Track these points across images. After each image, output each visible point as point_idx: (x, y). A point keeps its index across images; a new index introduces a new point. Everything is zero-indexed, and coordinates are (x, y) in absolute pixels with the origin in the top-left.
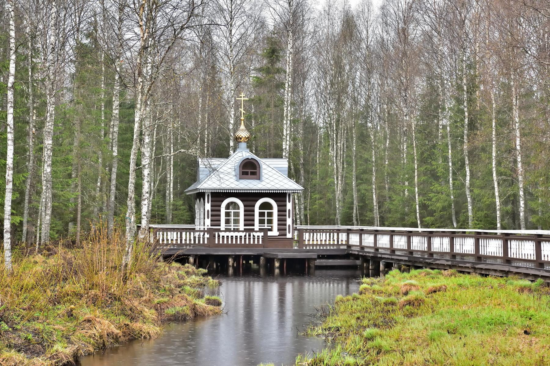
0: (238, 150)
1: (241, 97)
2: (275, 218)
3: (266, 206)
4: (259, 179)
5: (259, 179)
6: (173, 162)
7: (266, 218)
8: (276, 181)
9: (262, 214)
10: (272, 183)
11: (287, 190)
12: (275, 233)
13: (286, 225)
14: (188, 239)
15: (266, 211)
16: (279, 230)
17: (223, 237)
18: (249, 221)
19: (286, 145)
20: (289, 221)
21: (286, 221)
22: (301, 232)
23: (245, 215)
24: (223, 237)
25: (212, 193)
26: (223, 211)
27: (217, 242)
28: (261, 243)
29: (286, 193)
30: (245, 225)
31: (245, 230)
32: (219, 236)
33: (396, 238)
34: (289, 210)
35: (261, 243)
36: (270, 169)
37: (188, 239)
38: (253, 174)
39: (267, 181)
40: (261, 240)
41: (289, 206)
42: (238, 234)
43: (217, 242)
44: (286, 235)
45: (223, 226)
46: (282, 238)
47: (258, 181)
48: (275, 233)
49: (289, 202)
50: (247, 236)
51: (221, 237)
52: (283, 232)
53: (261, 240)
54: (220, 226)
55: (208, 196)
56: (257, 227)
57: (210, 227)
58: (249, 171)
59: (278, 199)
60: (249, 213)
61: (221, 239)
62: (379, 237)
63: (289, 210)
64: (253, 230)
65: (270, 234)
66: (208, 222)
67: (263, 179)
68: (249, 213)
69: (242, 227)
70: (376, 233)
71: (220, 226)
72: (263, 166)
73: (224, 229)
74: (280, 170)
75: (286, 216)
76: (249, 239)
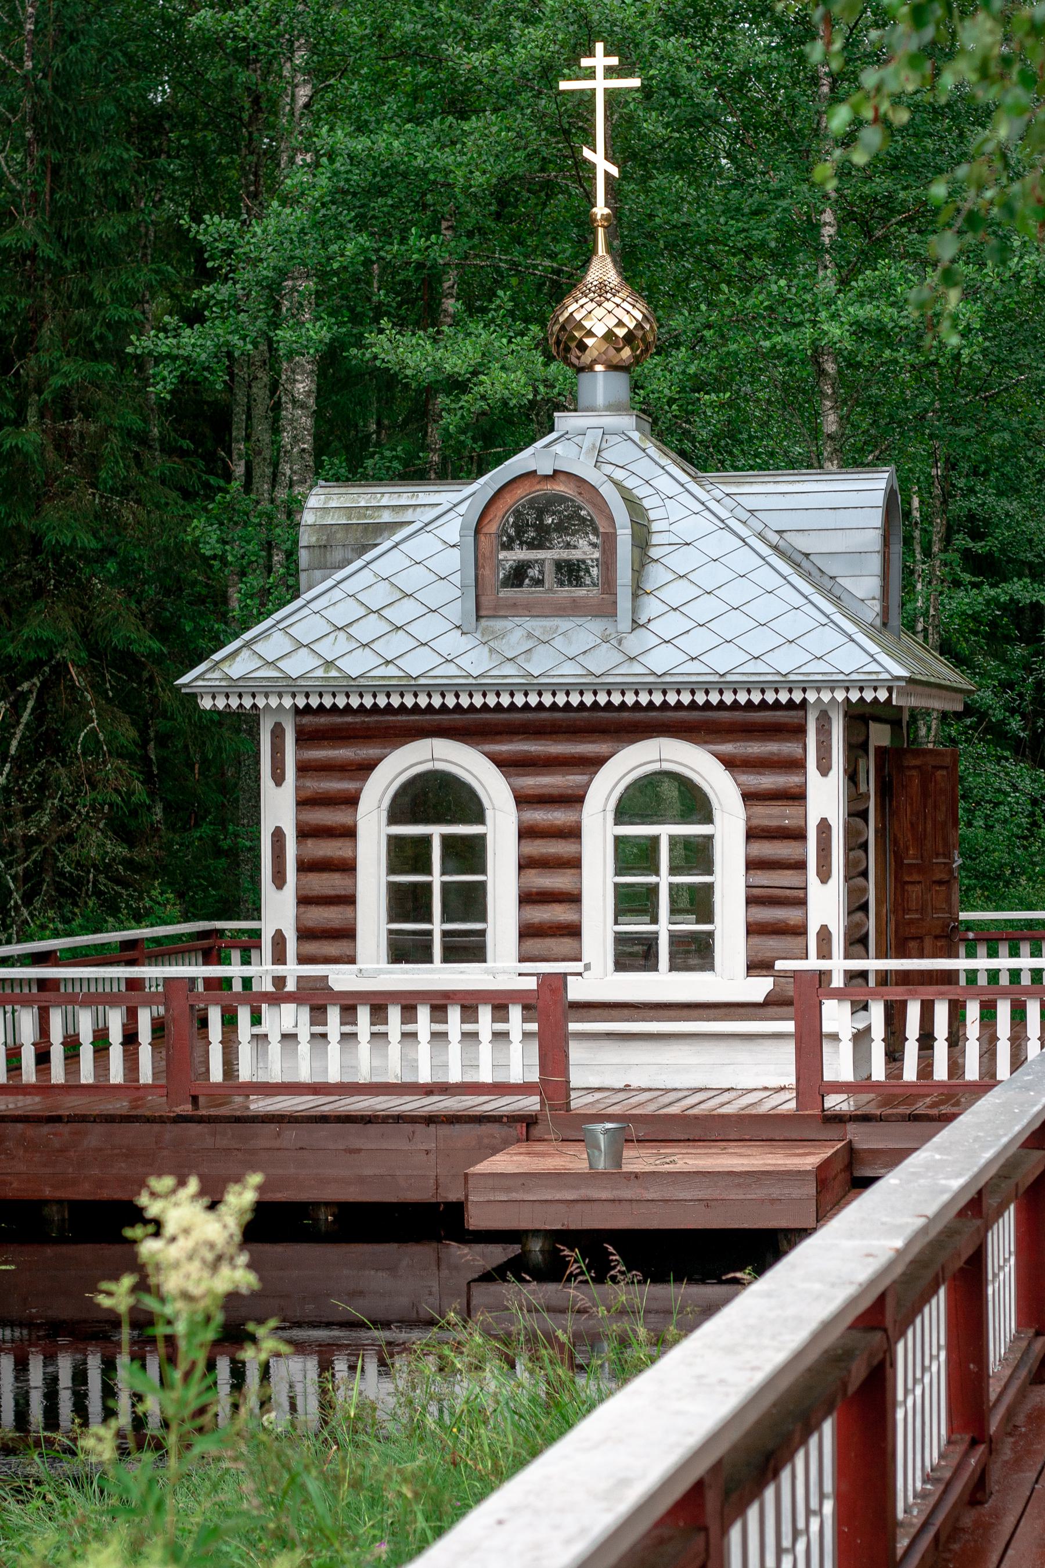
1: (590, 73)
4: (607, 610)
21: (802, 902)
27: (216, 1075)
28: (146, 1075)
43: (216, 1075)
47: (596, 626)
49: (279, 779)
55: (278, 733)
63: (824, 827)
75: (801, 866)
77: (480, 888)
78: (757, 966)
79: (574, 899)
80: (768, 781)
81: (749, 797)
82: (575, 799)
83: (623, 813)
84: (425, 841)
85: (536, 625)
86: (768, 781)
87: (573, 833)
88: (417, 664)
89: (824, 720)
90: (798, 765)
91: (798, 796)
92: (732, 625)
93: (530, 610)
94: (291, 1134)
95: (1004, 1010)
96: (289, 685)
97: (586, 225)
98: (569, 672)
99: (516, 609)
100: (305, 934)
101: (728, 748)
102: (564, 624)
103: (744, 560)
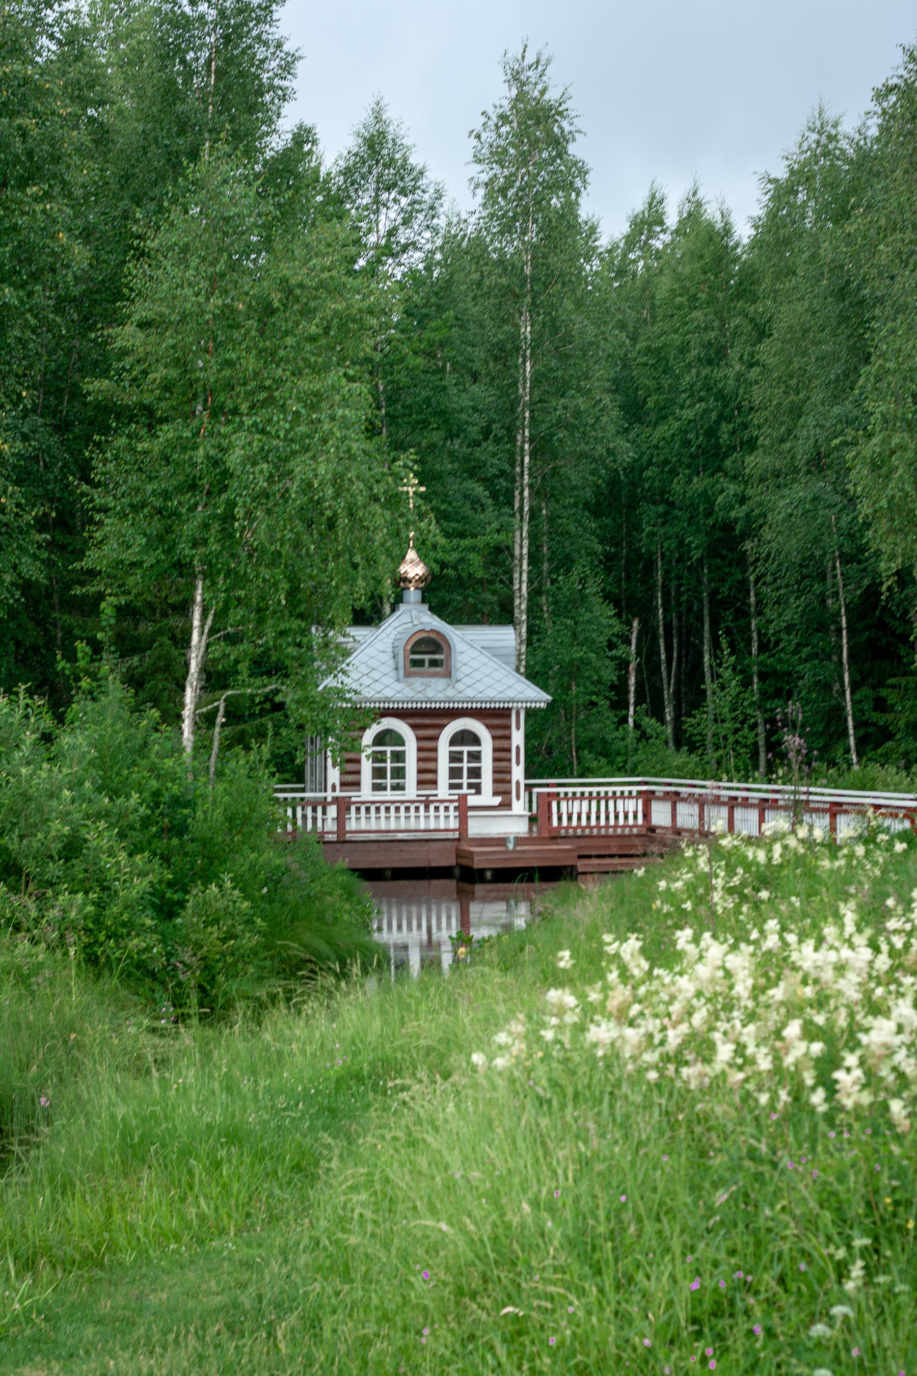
0: (402, 607)
2: (487, 765)
3: (465, 738)
5: (448, 675)
7: (389, 765)
9: (455, 757)
13: (510, 782)
15: (389, 749)
18: (427, 778)
19: (521, 605)
21: (510, 772)
26: (444, 748)
29: (509, 709)
30: (420, 783)
33: (682, 808)
34: (518, 748)
46: (579, 826)
56: (443, 791)
58: (426, 657)
59: (489, 721)
60: (427, 756)
62: (738, 813)
63: (518, 748)
68: (427, 756)
70: (674, 798)
75: (510, 760)
77: (403, 768)
78: (495, 793)
79: (435, 771)
80: (500, 733)
81: (419, 739)
82: (436, 738)
83: (453, 742)
84: (461, 753)
85: (425, 680)
86: (500, 733)
87: (435, 750)
88: (389, 693)
90: (509, 727)
91: (509, 738)
92: (488, 681)
93: (422, 675)
94: (402, 846)
95: (603, 803)
97: (848, 633)
98: (440, 696)
99: (415, 675)
100: (343, 784)
101: (411, 721)
102: (433, 680)
103: (482, 658)
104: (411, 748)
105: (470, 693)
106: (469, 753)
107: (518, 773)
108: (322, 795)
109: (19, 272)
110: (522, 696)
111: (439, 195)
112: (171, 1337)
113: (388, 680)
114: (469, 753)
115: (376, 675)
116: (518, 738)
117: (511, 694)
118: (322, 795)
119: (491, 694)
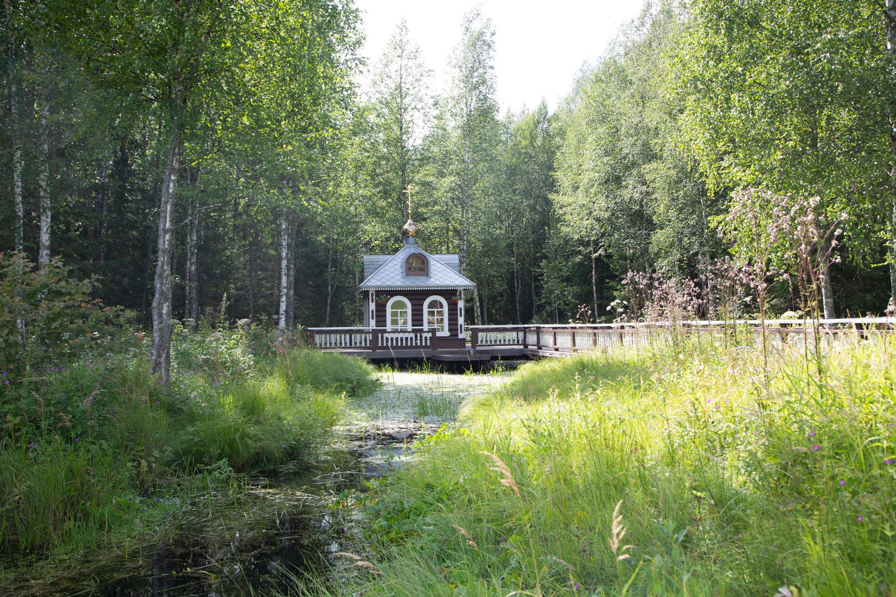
5: (427, 275)
6: (53, 234)
8: (446, 277)
9: (394, 314)
10: (442, 280)
11: (458, 286)
12: (446, 333)
14: (328, 342)
15: (399, 311)
16: (450, 330)
17: (426, 338)
20: (461, 320)
21: (457, 320)
22: (475, 332)
23: (412, 315)
24: (426, 338)
25: (464, 290)
27: (380, 345)
28: (428, 344)
29: (457, 290)
31: (414, 331)
32: (421, 337)
34: (461, 309)
35: (428, 344)
36: (439, 265)
37: (328, 342)
38: (421, 269)
39: (437, 277)
40: (428, 341)
41: (461, 304)
42: (404, 335)
43: (380, 345)
44: (457, 335)
45: (389, 327)
48: (446, 333)
50: (414, 338)
51: (423, 338)
52: (454, 332)
53: (428, 341)
54: (422, 326)
55: (372, 294)
56: (426, 327)
57: (375, 328)
59: (412, 297)
61: (424, 341)
63: (461, 309)
64: (421, 331)
65: (438, 334)
66: (373, 323)
67: (432, 275)
69: (410, 327)
71: (422, 326)
72: (431, 260)
73: (390, 330)
74: (450, 265)
76: (421, 340)
89: (460, 292)
96: (373, 287)
104: (446, 309)
105: (438, 283)
106: (401, 312)
107: (461, 320)
108: (368, 328)
109: (293, 106)
110: (462, 284)
111: (358, 43)
112: (68, 535)
113: (398, 277)
114: (401, 312)
115: (393, 275)
116: (461, 304)
117: (457, 283)
118: (368, 328)
119: (448, 283)
